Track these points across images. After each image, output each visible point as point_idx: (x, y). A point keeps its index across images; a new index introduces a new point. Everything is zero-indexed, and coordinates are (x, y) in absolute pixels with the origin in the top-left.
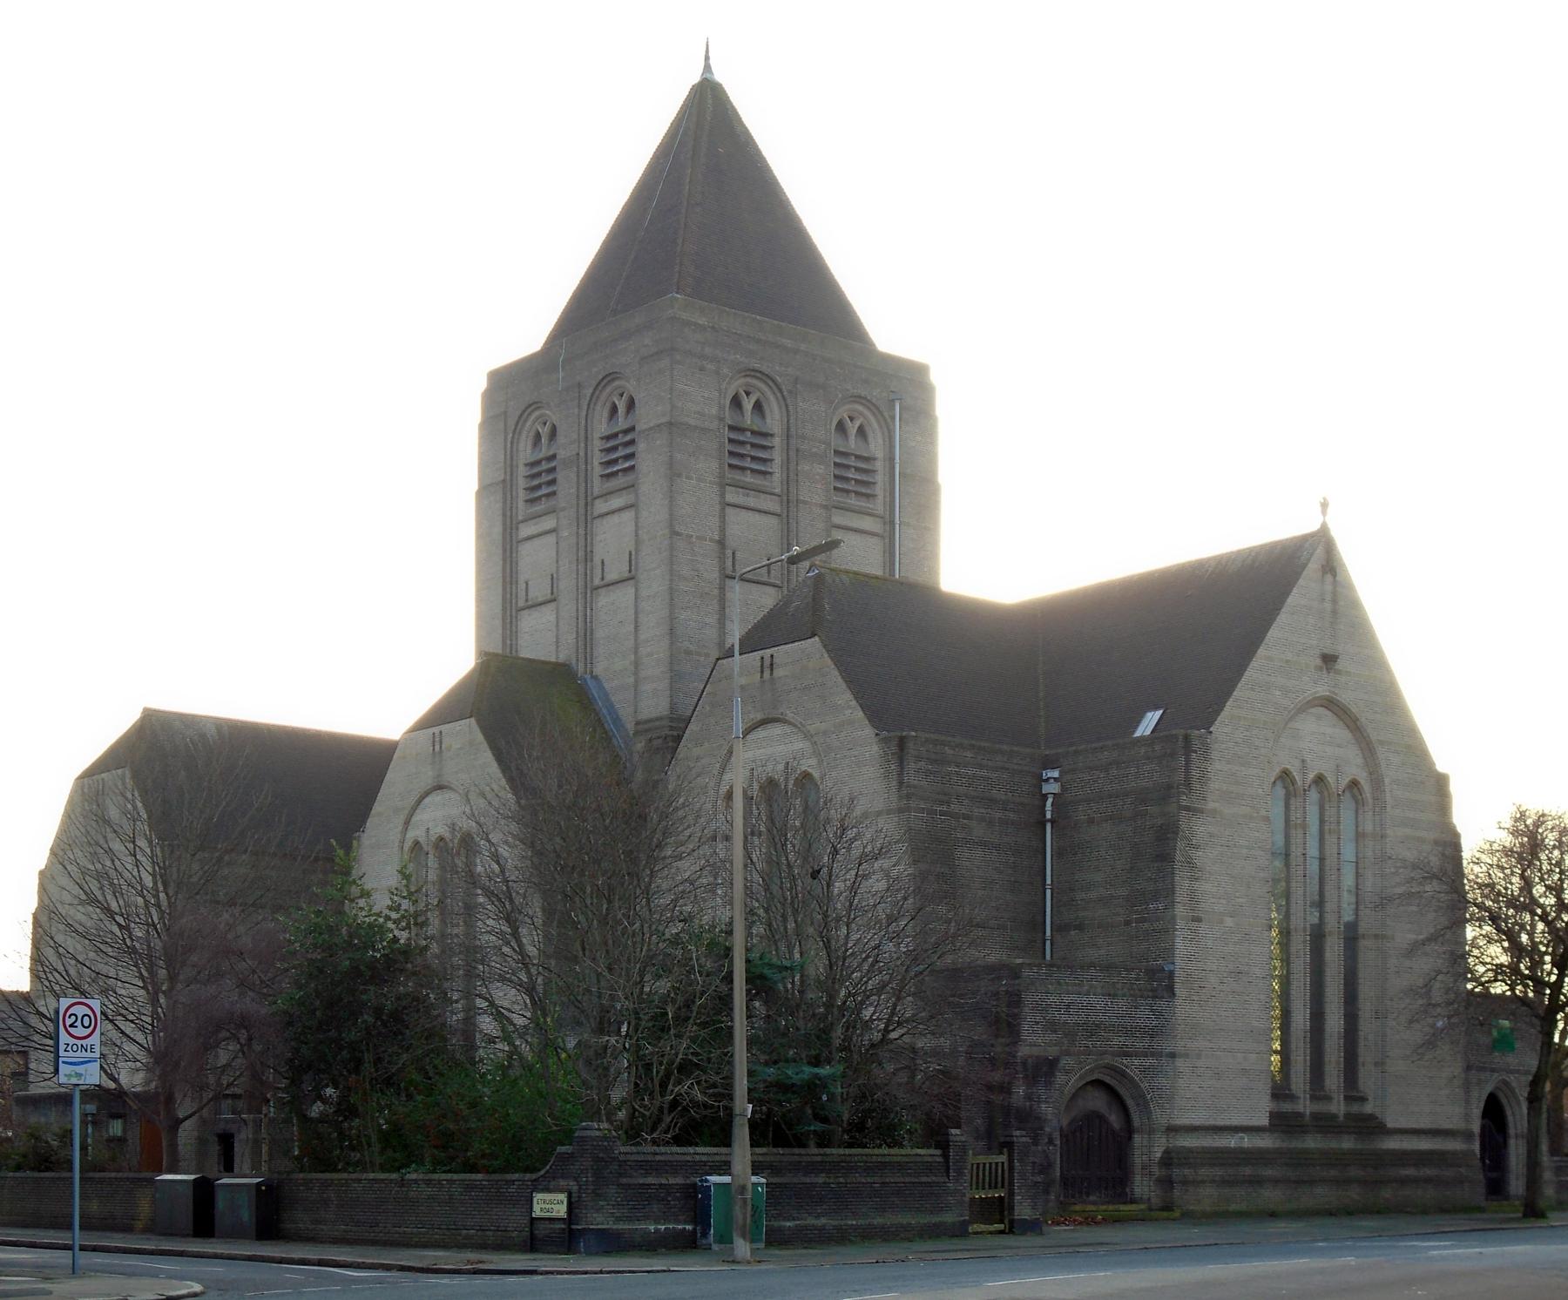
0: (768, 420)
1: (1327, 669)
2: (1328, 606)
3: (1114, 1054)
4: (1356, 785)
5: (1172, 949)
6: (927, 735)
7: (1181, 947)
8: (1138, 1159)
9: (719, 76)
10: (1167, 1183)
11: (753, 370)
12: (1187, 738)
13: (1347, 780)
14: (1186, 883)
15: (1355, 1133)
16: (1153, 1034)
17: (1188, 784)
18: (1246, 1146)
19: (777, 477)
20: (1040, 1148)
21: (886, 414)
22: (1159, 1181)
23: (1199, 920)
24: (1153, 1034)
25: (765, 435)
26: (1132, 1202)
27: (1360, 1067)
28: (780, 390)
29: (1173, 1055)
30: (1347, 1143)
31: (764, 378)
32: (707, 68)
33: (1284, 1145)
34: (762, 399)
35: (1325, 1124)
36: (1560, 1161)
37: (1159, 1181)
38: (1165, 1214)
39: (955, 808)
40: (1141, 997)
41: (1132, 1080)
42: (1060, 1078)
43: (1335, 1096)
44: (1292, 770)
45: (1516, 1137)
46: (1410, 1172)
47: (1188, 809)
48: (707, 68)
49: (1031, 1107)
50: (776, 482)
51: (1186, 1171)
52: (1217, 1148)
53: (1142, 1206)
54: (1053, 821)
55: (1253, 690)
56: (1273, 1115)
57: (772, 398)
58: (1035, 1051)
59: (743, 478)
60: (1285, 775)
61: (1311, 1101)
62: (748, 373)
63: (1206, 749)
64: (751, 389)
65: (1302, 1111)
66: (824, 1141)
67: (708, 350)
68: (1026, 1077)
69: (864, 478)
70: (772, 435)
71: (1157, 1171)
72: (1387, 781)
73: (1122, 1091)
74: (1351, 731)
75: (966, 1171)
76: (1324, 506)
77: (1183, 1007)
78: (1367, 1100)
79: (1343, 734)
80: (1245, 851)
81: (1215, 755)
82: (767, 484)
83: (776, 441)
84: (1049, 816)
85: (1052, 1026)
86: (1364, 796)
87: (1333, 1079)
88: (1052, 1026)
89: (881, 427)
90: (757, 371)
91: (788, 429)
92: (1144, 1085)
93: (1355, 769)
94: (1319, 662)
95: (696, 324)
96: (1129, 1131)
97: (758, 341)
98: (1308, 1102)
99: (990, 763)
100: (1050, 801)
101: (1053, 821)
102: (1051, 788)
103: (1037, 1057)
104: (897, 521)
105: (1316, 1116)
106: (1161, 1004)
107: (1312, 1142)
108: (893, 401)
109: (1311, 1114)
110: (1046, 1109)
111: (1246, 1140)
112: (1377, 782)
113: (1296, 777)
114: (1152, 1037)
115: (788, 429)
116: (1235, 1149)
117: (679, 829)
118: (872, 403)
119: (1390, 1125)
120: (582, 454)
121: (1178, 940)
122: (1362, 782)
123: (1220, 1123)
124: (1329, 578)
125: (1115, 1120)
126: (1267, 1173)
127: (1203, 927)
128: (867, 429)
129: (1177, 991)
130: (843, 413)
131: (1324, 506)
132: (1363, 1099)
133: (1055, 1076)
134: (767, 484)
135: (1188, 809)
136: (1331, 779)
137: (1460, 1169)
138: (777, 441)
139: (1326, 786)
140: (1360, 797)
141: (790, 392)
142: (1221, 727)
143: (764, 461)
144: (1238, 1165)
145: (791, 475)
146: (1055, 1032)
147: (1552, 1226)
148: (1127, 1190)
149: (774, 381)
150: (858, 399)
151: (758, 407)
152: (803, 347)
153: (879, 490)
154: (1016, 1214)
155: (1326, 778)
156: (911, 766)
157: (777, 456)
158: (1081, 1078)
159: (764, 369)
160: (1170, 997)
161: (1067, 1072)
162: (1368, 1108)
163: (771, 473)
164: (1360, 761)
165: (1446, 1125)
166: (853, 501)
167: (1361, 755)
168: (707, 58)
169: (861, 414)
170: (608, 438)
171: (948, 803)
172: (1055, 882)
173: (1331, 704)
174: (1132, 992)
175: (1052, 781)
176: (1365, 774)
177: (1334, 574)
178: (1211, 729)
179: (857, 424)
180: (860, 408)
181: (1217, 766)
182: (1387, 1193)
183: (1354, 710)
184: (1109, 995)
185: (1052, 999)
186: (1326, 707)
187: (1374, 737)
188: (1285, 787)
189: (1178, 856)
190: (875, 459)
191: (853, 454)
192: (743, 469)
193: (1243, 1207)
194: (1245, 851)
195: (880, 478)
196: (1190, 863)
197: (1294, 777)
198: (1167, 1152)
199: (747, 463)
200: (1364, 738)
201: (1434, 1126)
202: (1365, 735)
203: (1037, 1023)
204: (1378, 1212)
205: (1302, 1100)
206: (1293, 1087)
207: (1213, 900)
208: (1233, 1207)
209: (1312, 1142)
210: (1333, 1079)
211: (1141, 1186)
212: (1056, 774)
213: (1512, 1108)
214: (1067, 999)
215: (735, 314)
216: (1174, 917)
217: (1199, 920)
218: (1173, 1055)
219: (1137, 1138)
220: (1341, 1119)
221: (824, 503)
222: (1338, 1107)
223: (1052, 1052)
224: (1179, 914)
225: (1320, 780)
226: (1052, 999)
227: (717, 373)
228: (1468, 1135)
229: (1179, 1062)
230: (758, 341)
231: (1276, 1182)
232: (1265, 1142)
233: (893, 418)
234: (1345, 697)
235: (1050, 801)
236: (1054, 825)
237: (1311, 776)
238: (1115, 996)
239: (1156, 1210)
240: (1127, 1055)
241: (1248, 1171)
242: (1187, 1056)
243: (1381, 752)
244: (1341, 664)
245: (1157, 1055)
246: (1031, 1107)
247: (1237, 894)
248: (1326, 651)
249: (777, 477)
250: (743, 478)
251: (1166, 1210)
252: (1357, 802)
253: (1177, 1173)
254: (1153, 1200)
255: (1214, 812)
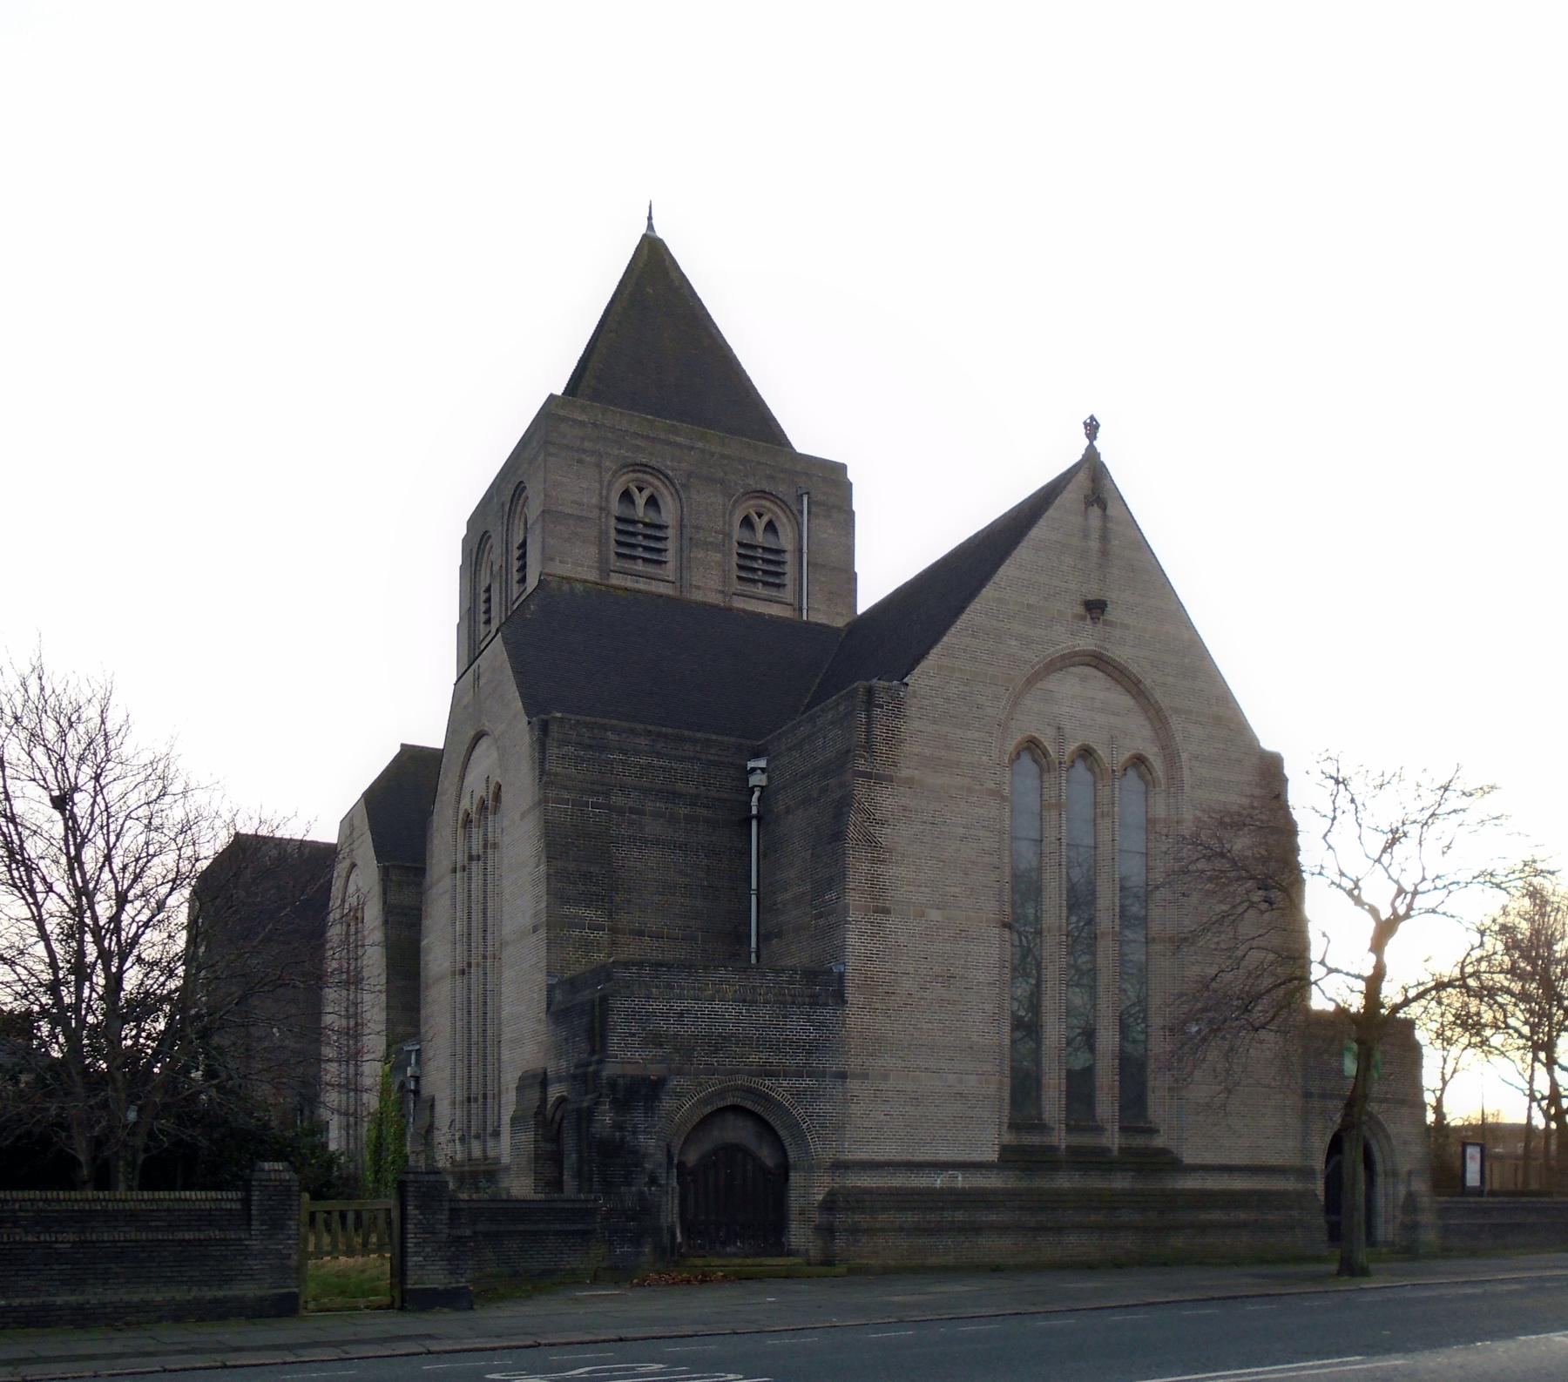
0: (663, 514)
1: (1092, 618)
2: (1094, 544)
3: (751, 1074)
4: (1143, 762)
5: (843, 948)
6: (578, 717)
7: (855, 942)
8: (795, 1201)
9: (660, 232)
10: (827, 1232)
11: (641, 465)
12: (870, 692)
13: (1127, 755)
14: (865, 866)
15: (1132, 1170)
16: (812, 1048)
17: (869, 746)
18: (960, 1185)
19: (671, 565)
20: (634, 1189)
21: (794, 508)
22: (818, 1228)
23: (886, 911)
24: (812, 1048)
25: (661, 527)
26: (790, 1254)
27: (1150, 1093)
28: (673, 484)
29: (842, 1076)
30: (1121, 1182)
31: (654, 472)
32: (650, 226)
33: (1024, 1184)
34: (656, 494)
35: (1090, 1160)
36: (1447, 1202)
37: (818, 1228)
38: (823, 1269)
39: (617, 800)
40: (793, 1003)
41: (780, 1105)
42: (667, 1103)
43: (1108, 1126)
44: (1043, 740)
45: (1386, 1175)
46: (1217, 1216)
47: (868, 776)
48: (650, 226)
49: (622, 1138)
50: (669, 571)
51: (857, 1218)
52: (913, 1188)
53: (798, 1260)
54: (759, 818)
55: (974, 636)
56: (1004, 1149)
57: (665, 492)
58: (630, 1070)
59: (635, 567)
60: (1032, 746)
61: (1008, 1127)
62: (637, 468)
63: (898, 707)
64: (644, 485)
65: (1110, 1145)
66: (103, 1180)
67: (587, 445)
68: (614, 1101)
69: (772, 568)
70: (667, 527)
71: (817, 1218)
72: (1184, 756)
73: (771, 1119)
74: (1134, 698)
75: (291, 1223)
76: (1092, 428)
77: (857, 1016)
78: (1158, 1131)
79: (1123, 700)
80: (961, 831)
81: (912, 711)
82: (661, 572)
83: (671, 532)
84: (754, 811)
85: (656, 1040)
86: (1154, 775)
87: (1106, 1106)
88: (656, 1040)
89: (790, 521)
90: (646, 466)
91: (682, 520)
92: (798, 1112)
93: (1139, 737)
94: (1080, 610)
95: (574, 420)
96: (784, 1169)
97: (647, 438)
98: (1063, 1134)
99: (674, 752)
100: (756, 794)
101: (759, 818)
102: (757, 780)
103: (632, 1077)
104: (805, 606)
105: (1073, 1150)
106: (827, 1013)
107: (1064, 1181)
108: (802, 495)
109: (1068, 1147)
110: (649, 1143)
111: (960, 1179)
112: (1172, 759)
113: (1049, 748)
114: (809, 1052)
115: (682, 520)
116: (941, 1188)
117: (1138, 1008)
118: (778, 498)
119: (1188, 1159)
120: (504, 565)
121: (850, 935)
122: (1151, 758)
123: (918, 1157)
124: (1095, 511)
125: (767, 1156)
126: (989, 1219)
127: (892, 922)
128: (777, 524)
129: (849, 997)
130: (749, 507)
131: (1092, 428)
132: (1152, 1131)
133: (660, 1101)
134: (661, 572)
135: (868, 776)
136: (1102, 752)
137: (1292, 1213)
138: (670, 533)
139: (1096, 761)
140: (1149, 777)
141: (683, 486)
142: (922, 678)
143: (659, 551)
144: (943, 1209)
145: (685, 562)
146: (661, 1045)
147: (1362, 1289)
148: (783, 1239)
149: (667, 477)
150: (763, 494)
151: (652, 502)
152: (700, 445)
153: (788, 580)
154: (409, 1282)
155: (1095, 751)
156: (553, 751)
157: (671, 545)
158: (706, 1101)
159: (653, 463)
160: (837, 1004)
161: (679, 1095)
162: (1159, 1142)
163: (665, 562)
164: (1147, 732)
165: (1273, 1160)
166: (760, 590)
167: (1149, 727)
168: (650, 218)
169: (769, 510)
170: (490, 537)
171: (607, 795)
172: (761, 889)
173: (1099, 661)
174: (781, 998)
175: (759, 771)
176: (1156, 749)
177: (1103, 507)
178: (905, 680)
179: (765, 519)
180: (768, 504)
181: (916, 725)
182: (1178, 1241)
183: (1134, 668)
184: (744, 1001)
185: (654, 1006)
186: (1095, 667)
187: (1164, 702)
188: (1035, 761)
189: (852, 832)
190: (784, 551)
191: (760, 547)
192: (634, 558)
193: (950, 1259)
194: (961, 831)
195: (789, 569)
196: (871, 842)
197: (1045, 747)
198: (832, 1194)
199: (639, 552)
200: (1152, 705)
201: (1256, 1162)
202: (1153, 702)
203: (634, 1035)
204: (1165, 1264)
205: (1056, 1132)
206: (1046, 1116)
207: (911, 888)
208: (933, 1261)
209: (1064, 1181)
210: (1106, 1106)
211: (799, 1235)
212: (762, 763)
213: (553, 1118)
214: (679, 1006)
215: (621, 413)
216: (846, 907)
217: (886, 911)
218: (842, 1076)
219: (795, 1178)
220: (1116, 1153)
221: (720, 588)
222: (1112, 1139)
223: (655, 1071)
224: (851, 902)
225: (1086, 753)
226: (654, 1006)
227: (599, 466)
228: (1305, 1173)
229: (853, 1085)
230: (647, 438)
231: (1002, 1229)
232: (993, 1181)
233: (802, 512)
234: (1121, 654)
235: (756, 794)
236: (762, 822)
237: (1072, 747)
238: (753, 1002)
239: (816, 1264)
240: (770, 1074)
241: (960, 1216)
242: (865, 1076)
243: (1175, 722)
244: (1112, 613)
245: (818, 1075)
246: (622, 1138)
247: (947, 882)
248: (1090, 598)
249: (671, 565)
250: (635, 567)
251: (826, 1265)
252: (1146, 783)
253: (842, 1219)
254: (812, 1253)
255: (910, 782)
